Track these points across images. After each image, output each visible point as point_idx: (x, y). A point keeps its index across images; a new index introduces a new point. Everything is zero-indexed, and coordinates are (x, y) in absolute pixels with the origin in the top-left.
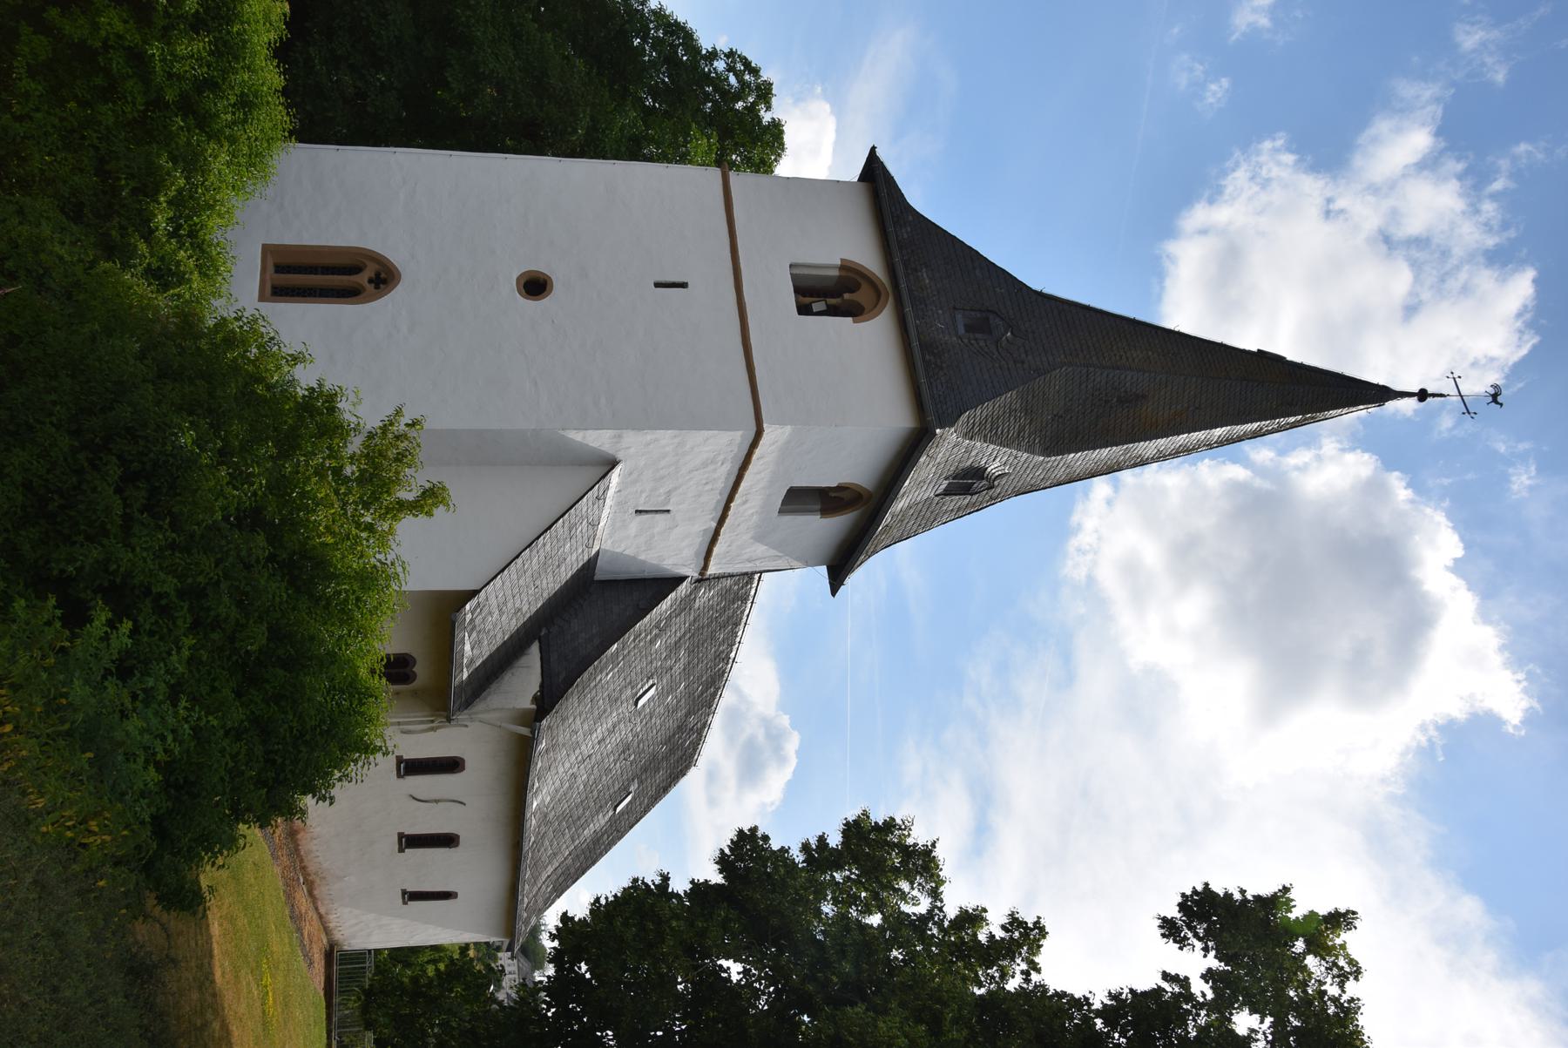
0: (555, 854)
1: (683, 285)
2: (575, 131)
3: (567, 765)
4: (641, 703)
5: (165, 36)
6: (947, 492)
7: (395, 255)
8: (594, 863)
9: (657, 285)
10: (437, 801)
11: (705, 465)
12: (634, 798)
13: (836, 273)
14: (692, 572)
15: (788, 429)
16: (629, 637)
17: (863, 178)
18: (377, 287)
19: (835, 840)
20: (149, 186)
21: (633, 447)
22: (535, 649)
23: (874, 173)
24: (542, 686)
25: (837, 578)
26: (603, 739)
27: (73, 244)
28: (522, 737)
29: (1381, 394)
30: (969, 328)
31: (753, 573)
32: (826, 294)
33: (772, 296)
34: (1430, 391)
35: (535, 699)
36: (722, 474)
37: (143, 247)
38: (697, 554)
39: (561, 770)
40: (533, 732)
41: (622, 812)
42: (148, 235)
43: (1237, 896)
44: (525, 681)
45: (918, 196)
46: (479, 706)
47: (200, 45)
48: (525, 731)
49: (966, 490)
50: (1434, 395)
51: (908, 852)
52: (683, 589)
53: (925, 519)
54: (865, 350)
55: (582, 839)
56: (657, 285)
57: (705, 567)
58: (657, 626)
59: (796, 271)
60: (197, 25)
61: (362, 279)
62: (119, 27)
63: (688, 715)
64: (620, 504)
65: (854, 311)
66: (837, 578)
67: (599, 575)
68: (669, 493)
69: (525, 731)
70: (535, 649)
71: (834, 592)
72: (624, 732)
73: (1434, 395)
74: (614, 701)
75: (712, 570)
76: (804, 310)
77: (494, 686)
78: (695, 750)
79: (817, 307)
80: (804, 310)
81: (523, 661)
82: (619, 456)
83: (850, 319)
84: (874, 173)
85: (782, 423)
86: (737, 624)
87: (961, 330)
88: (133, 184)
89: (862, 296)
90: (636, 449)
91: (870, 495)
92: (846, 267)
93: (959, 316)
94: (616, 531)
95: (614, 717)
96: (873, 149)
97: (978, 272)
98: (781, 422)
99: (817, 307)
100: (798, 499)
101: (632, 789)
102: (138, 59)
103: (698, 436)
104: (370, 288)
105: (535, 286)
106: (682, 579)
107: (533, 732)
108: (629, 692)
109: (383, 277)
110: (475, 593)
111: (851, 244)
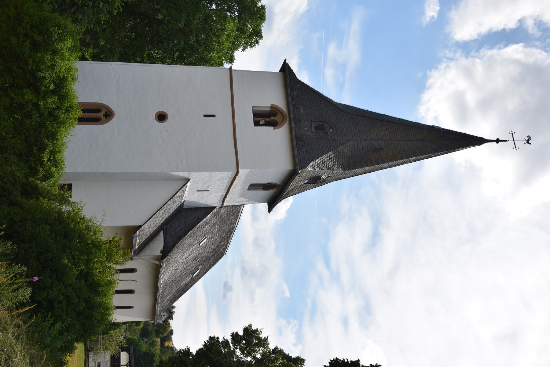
0: (170, 293)
1: (214, 116)
2: (180, 22)
3: (174, 267)
4: (201, 244)
5: (44, 99)
6: (307, 183)
7: (113, 106)
8: (186, 292)
9: (205, 116)
10: (127, 281)
11: (220, 179)
12: (201, 270)
13: (269, 109)
14: (218, 205)
15: (248, 170)
16: (196, 228)
18: (106, 118)
19: (241, 333)
20: (42, 149)
21: (194, 176)
22: (162, 233)
23: (285, 68)
24: (164, 247)
25: (270, 208)
26: (187, 257)
27: (21, 170)
28: (157, 265)
29: (479, 141)
30: (317, 128)
31: (241, 205)
32: (265, 118)
33: (246, 118)
35: (162, 252)
36: (226, 182)
37: (41, 169)
38: (219, 201)
39: (171, 269)
40: (160, 263)
41: (196, 275)
42: (42, 164)
43: (346, 361)
44: (158, 246)
46: (142, 254)
47: (55, 99)
48: (158, 263)
49: (315, 182)
51: (260, 339)
52: (215, 210)
53: (302, 189)
54: (278, 138)
55: (180, 286)
56: (205, 116)
57: (223, 204)
58: (206, 222)
59: (254, 109)
60: (53, 92)
61: (101, 115)
62: (31, 97)
63: (221, 242)
64: (191, 189)
65: (274, 124)
66: (270, 208)
68: (208, 186)
69: (158, 263)
70: (162, 233)
71: (269, 212)
72: (196, 253)
74: (190, 246)
75: (225, 204)
76: (257, 124)
78: (224, 251)
79: (262, 122)
80: (257, 124)
81: (158, 238)
82: (190, 178)
83: (272, 128)
84: (285, 68)
85: (246, 168)
86: (238, 213)
87: (313, 129)
88: (37, 148)
89: (278, 118)
90: (194, 176)
91: (279, 185)
92: (273, 107)
93: (313, 125)
94: (191, 196)
95: (191, 250)
96: (285, 60)
97: (322, 105)
98: (245, 168)
99: (262, 122)
100: (253, 187)
101: (200, 268)
102: (36, 105)
103: (215, 174)
104: (104, 118)
105: (162, 117)
107: (160, 263)
108: (196, 242)
109: (109, 115)
110: (140, 227)
111: (274, 97)
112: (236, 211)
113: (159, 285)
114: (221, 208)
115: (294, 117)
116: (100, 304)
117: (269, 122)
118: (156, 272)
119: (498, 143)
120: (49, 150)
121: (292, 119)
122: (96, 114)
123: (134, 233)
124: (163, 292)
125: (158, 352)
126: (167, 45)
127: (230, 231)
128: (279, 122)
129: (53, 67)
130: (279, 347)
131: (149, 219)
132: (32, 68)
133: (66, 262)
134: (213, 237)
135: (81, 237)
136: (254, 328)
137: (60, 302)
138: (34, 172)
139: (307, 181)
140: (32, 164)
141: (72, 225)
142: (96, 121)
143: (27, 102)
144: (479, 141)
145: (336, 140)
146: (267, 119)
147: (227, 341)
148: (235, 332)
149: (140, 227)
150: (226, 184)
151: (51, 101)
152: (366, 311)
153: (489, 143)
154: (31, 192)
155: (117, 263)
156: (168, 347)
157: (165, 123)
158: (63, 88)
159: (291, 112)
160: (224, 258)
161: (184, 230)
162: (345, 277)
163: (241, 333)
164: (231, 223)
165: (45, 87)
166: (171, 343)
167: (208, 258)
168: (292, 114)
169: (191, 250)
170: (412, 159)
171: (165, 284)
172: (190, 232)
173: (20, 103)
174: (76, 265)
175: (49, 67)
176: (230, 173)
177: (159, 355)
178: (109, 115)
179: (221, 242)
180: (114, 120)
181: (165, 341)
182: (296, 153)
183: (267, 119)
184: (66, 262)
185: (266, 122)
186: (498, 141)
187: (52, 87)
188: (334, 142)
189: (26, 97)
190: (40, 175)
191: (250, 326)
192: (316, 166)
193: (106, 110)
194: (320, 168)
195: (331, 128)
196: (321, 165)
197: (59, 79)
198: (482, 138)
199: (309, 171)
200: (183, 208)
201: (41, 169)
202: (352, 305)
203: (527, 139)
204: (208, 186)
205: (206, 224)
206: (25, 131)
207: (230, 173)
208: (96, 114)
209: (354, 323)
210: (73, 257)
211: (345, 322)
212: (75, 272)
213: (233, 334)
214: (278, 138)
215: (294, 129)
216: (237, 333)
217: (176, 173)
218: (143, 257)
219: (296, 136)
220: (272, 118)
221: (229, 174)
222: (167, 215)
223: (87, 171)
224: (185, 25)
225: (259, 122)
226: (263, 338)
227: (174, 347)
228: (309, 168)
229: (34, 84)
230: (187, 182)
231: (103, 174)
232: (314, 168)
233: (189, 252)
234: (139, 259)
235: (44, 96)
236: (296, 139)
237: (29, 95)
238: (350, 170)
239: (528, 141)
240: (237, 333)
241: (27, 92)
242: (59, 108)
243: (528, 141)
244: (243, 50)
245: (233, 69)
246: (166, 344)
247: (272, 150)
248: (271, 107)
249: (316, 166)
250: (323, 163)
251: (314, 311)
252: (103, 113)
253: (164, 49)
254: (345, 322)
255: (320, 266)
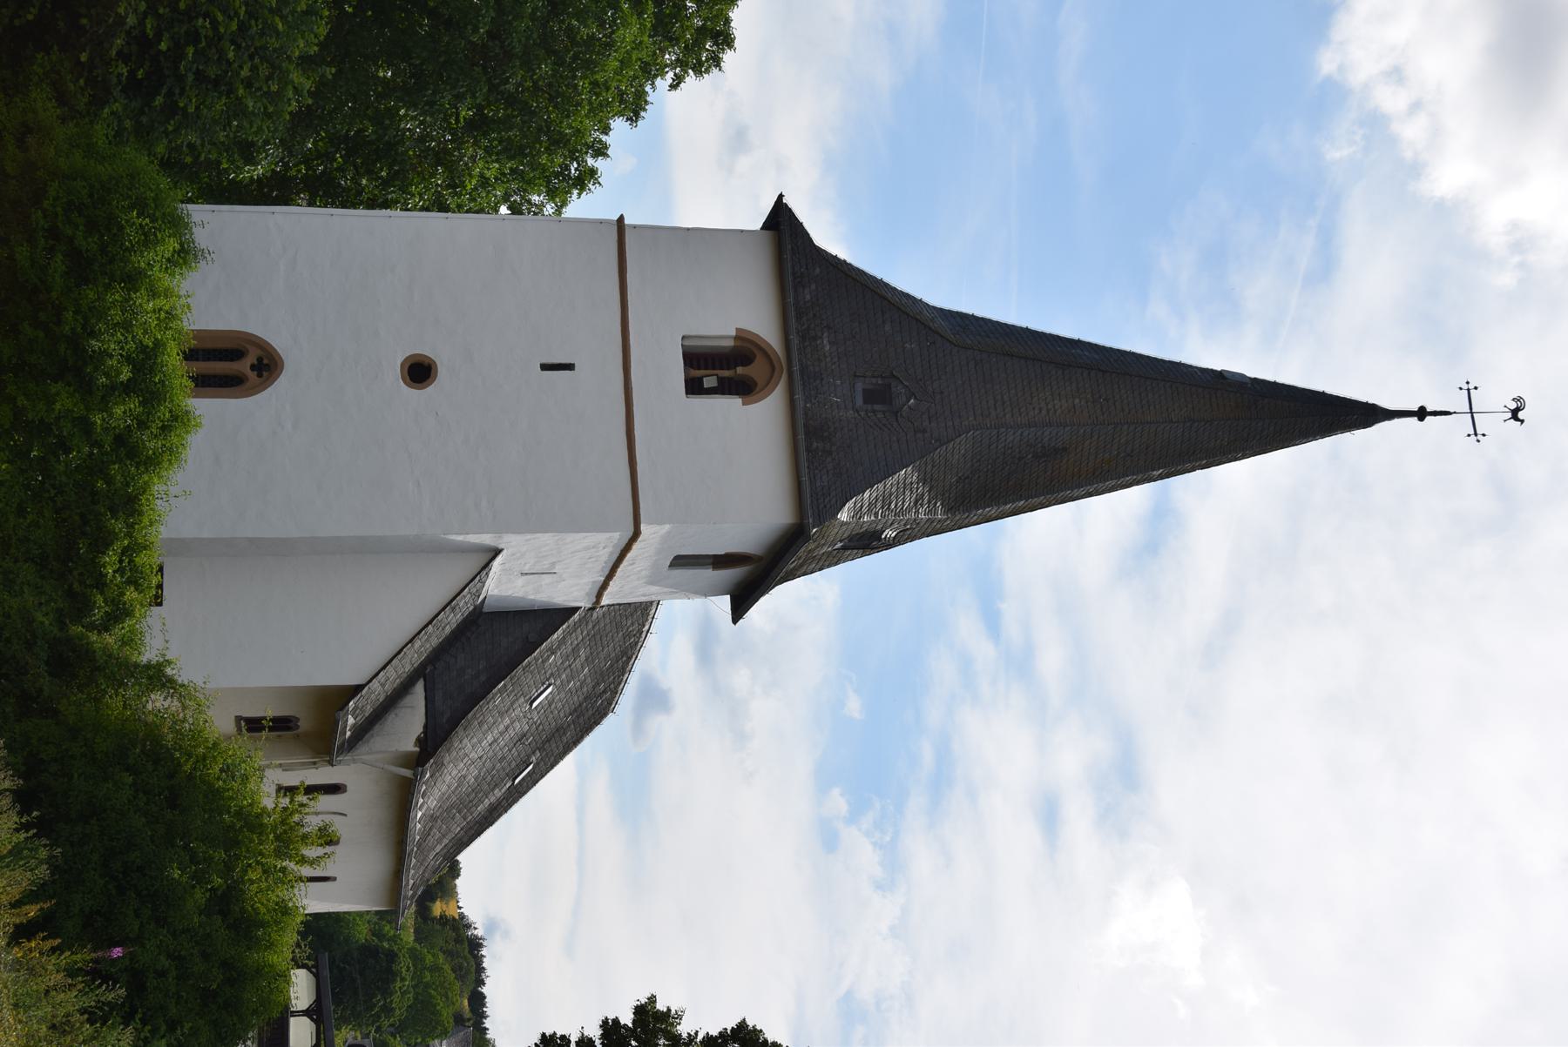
1: (569, 367)
2: (475, 30)
5: (105, 407)
6: (844, 548)
7: (279, 341)
9: (545, 367)
11: (587, 548)
13: (731, 343)
15: (667, 527)
17: (766, 226)
18: (260, 376)
19: (627, 1019)
20: (102, 542)
21: (512, 544)
22: (419, 688)
23: (781, 220)
24: (426, 727)
25: (738, 612)
29: (1364, 415)
30: (869, 397)
32: (717, 369)
33: (662, 370)
34: (1415, 419)
35: (419, 741)
36: (605, 555)
40: (415, 775)
42: (100, 583)
44: (409, 724)
45: (827, 236)
47: (134, 404)
48: (408, 773)
50: (1435, 413)
54: (753, 430)
56: (545, 367)
57: (599, 595)
59: (687, 343)
60: (128, 388)
61: (244, 366)
65: (745, 389)
66: (738, 612)
67: (485, 610)
68: (553, 564)
69: (408, 773)
70: (419, 688)
71: (735, 621)
73: (1435, 413)
75: (605, 601)
76: (694, 387)
77: (377, 727)
79: (709, 382)
80: (694, 387)
81: (407, 700)
83: (737, 401)
84: (781, 220)
86: (629, 658)
87: (859, 401)
89: (755, 371)
90: (512, 544)
92: (742, 337)
94: (504, 585)
95: (507, 721)
96: (781, 196)
97: (888, 327)
100: (680, 562)
102: (85, 426)
103: (570, 537)
104: (252, 375)
105: (419, 372)
106: (577, 609)
107: (415, 775)
109: (267, 366)
111: (745, 309)
112: (636, 618)
113: (411, 825)
114: (592, 609)
115: (803, 371)
116: (259, 971)
117: (730, 379)
118: (403, 796)
119: (1421, 419)
120: (118, 546)
121: (797, 376)
122: (238, 365)
123: (342, 709)
124: (426, 834)
125: (409, 937)
126: (434, 93)
127: (624, 653)
128: (760, 383)
129: (127, 326)
130: (750, 1023)
131: (384, 668)
132: (73, 330)
133: (176, 874)
134: (571, 678)
135: (215, 798)
136: (661, 1006)
137: (162, 974)
138: (80, 607)
139: (839, 545)
140: (76, 585)
141: (187, 768)
142: (229, 384)
143: (58, 419)
144: (1364, 415)
145: (924, 431)
146: (726, 373)
147: (590, 1040)
148: (611, 1017)
149: (358, 689)
150: (604, 558)
151: (123, 411)
152: (1123, 778)
153: (1396, 421)
154: (75, 663)
155: (303, 860)
156: (444, 920)
157: (430, 390)
158: (152, 371)
159: (795, 354)
160: (610, 720)
161: (483, 678)
162: (1051, 660)
163: (627, 1019)
164: (627, 636)
165: (107, 375)
166: (452, 904)
167: (560, 730)
168: (796, 362)
169: (507, 721)
170: (1156, 473)
171: (432, 818)
172: (504, 681)
173: (42, 421)
174: (200, 878)
175: (116, 325)
176: (617, 535)
177: (412, 951)
178: (267, 366)
179: (598, 684)
180: (282, 383)
181: (433, 900)
182: (805, 479)
183: (726, 373)
184: (176, 874)
185: (721, 380)
186: (1422, 414)
187: (126, 374)
188: (919, 435)
189: (58, 406)
190: (98, 615)
191: (652, 999)
192: (865, 509)
193: (259, 352)
194: (876, 514)
195: (913, 395)
196: (879, 505)
197: (143, 348)
198: (1374, 406)
199: (843, 524)
200: (481, 613)
201: (99, 600)
202: (1075, 755)
203: (1513, 406)
204: (553, 564)
205: (554, 651)
206: (53, 492)
207: (617, 535)
208: (238, 365)
209: (1078, 816)
210: (194, 860)
211: (1049, 815)
212: (200, 896)
213: (605, 1022)
214: (753, 430)
215: (800, 404)
216: (616, 1021)
217: (460, 538)
218: (364, 757)
219: (805, 426)
220: (740, 370)
221: (617, 538)
222: (435, 642)
223: (205, 535)
224: (492, 35)
225: (700, 380)
226: (685, 1035)
227: (462, 916)
228: (844, 516)
229: (76, 367)
230: (493, 558)
231: (251, 540)
232: (858, 513)
233: (502, 727)
234: (354, 761)
235: (103, 397)
236: (806, 434)
237: (66, 401)
238: (969, 511)
239: (1515, 414)
240: (616, 1021)
241: (58, 394)
242: (142, 425)
243: (1515, 414)
244: (674, 87)
245: (627, 222)
246: (437, 908)
247: (739, 459)
248: (736, 338)
249: (865, 509)
250: (886, 500)
251: (940, 783)
252: (251, 359)
253: (427, 103)
254: (1049, 815)
255: (967, 628)
